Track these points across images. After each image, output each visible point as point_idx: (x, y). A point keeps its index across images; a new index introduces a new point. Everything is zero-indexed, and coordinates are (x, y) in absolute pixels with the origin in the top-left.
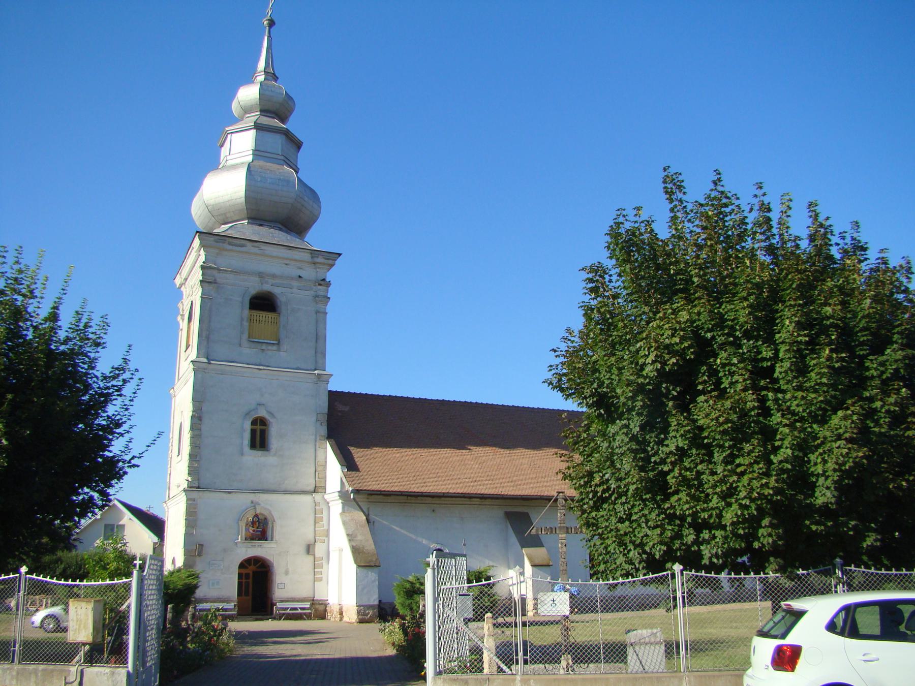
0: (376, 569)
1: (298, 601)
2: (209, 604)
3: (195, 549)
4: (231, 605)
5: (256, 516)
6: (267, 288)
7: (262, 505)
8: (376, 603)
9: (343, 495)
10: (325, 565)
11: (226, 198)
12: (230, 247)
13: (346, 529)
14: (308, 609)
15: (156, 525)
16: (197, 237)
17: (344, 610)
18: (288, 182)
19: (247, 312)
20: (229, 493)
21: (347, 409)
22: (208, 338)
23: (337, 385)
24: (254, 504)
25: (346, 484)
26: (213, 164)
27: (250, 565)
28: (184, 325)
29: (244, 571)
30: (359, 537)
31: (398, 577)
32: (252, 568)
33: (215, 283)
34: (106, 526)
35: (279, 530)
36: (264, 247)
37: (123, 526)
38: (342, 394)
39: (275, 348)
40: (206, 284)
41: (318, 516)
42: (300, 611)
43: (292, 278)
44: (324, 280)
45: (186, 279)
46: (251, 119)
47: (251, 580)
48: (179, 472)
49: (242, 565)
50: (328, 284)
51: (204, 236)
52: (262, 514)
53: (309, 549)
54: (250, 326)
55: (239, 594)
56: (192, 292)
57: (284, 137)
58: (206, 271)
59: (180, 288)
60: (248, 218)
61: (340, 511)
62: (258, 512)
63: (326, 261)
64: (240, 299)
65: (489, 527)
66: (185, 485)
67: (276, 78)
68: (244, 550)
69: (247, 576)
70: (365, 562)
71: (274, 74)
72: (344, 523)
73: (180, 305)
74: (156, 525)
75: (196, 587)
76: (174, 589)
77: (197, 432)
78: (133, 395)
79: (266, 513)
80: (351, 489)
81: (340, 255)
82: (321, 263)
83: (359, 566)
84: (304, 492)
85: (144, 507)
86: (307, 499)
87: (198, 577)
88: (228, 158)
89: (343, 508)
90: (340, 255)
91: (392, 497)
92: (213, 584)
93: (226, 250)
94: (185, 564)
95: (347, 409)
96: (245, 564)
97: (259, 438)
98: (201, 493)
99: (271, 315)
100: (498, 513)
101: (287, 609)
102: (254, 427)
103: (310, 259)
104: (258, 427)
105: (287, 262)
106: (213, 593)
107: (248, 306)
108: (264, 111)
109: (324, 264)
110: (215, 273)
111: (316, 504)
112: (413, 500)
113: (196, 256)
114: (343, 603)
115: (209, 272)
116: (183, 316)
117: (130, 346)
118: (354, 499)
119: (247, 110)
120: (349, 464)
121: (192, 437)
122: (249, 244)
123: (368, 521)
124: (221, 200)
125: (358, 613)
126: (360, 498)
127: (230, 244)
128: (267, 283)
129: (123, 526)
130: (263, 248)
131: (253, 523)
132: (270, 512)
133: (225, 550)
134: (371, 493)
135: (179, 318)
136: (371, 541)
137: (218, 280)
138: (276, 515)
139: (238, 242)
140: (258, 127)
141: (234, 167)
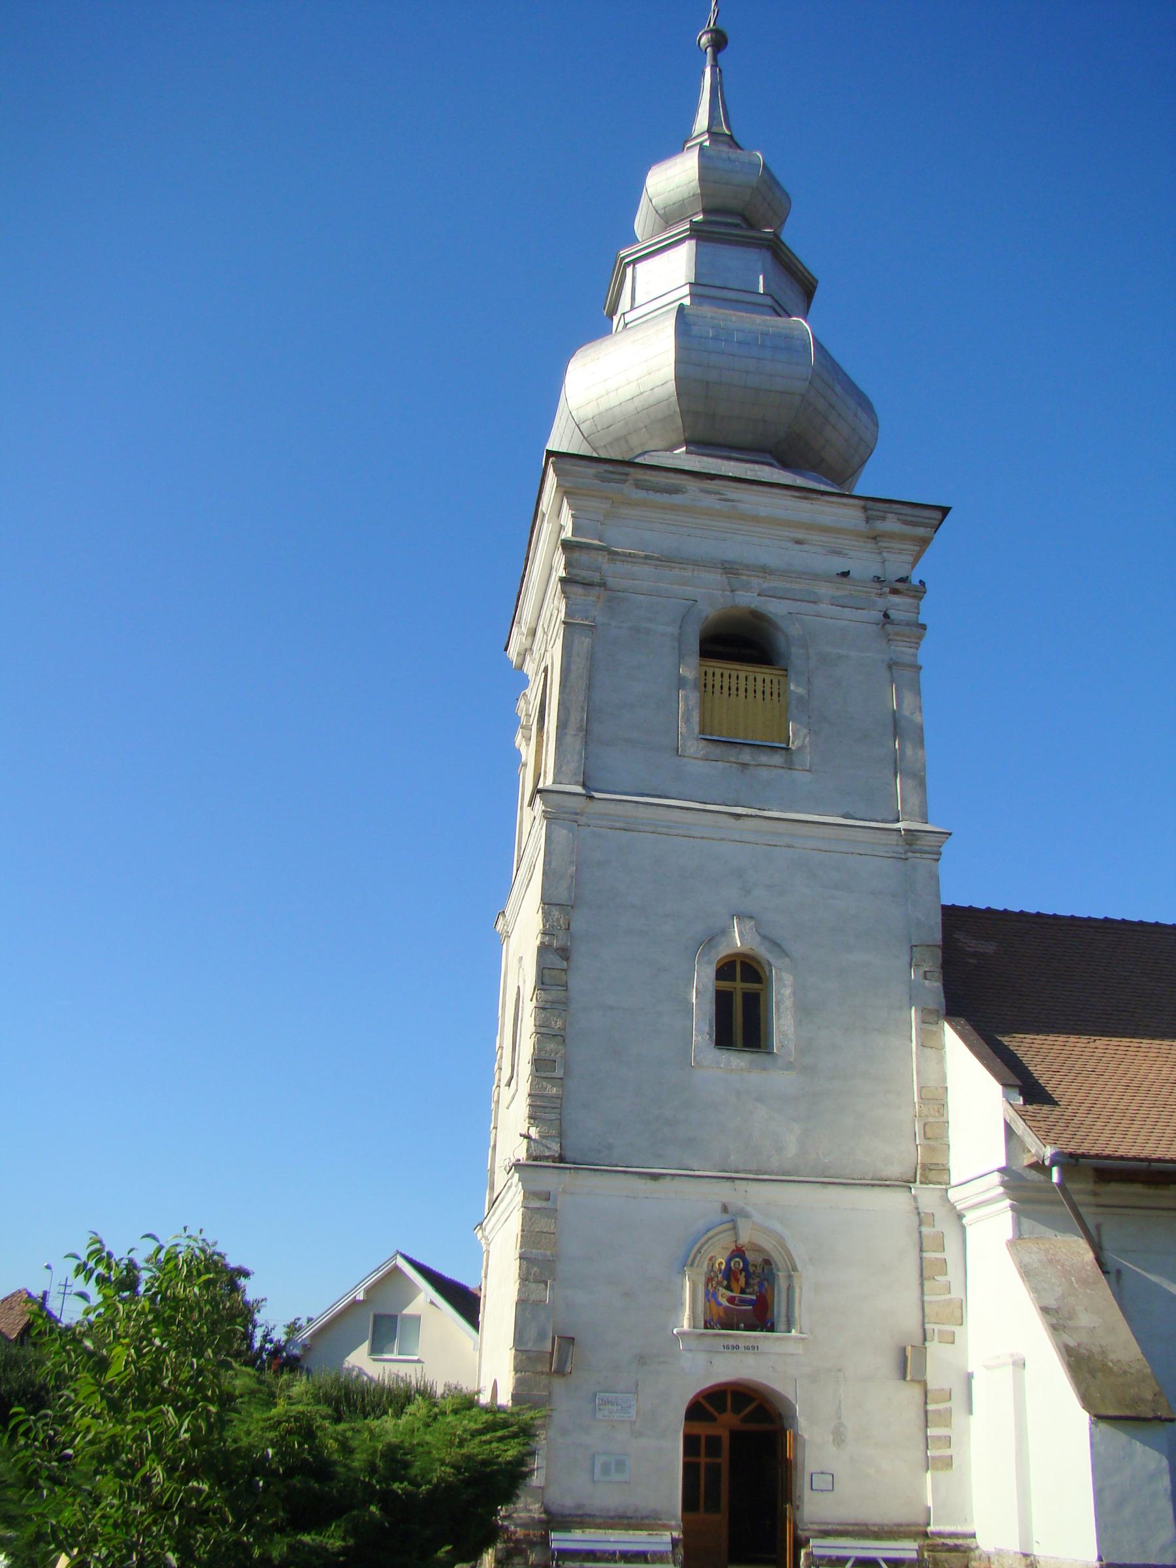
3: (548, 1353)
4: (663, 1540)
5: (739, 1252)
6: (747, 599)
7: (757, 1217)
9: (1022, 1187)
10: (957, 1417)
11: (627, 392)
12: (641, 494)
15: (466, 1302)
19: (690, 670)
20: (655, 1177)
21: (989, 948)
22: (587, 732)
23: (948, 902)
24: (731, 1216)
26: (595, 318)
27: (722, 1409)
28: (528, 753)
29: (703, 1429)
30: (1085, 1319)
32: (727, 1422)
33: (603, 585)
34: (377, 1318)
35: (810, 1295)
37: (417, 1319)
38: (970, 913)
39: (777, 759)
40: (579, 590)
41: (931, 1254)
43: (816, 577)
44: (903, 580)
45: (533, 633)
47: (724, 1460)
48: (512, 1128)
49: (697, 1411)
50: (919, 591)
51: (567, 465)
52: (759, 1249)
53: (908, 1363)
54: (702, 702)
55: (690, 1503)
57: (768, 255)
58: (576, 555)
59: (520, 667)
60: (688, 442)
61: (1008, 1232)
62: (744, 1239)
63: (908, 530)
64: (673, 630)
68: (701, 1358)
69: (713, 1444)
71: (731, 137)
72: (1027, 1273)
73: (522, 704)
74: (466, 1302)
77: (555, 994)
79: (768, 1244)
80: (1048, 1151)
81: (945, 511)
82: (891, 536)
83: (1099, 1418)
84: (882, 1183)
86: (896, 1200)
89: (1017, 1225)
90: (945, 511)
92: (606, 1469)
94: (515, 1397)
95: (989, 948)
96: (707, 1406)
97: (741, 1019)
98: (567, 1177)
99: (762, 674)
102: (726, 985)
103: (862, 525)
104: (739, 986)
106: (606, 1498)
107: (696, 647)
109: (902, 537)
110: (602, 559)
111: (921, 1218)
113: (557, 519)
114: (1037, 1551)
115: (583, 557)
118: (1061, 1185)
119: (668, 217)
120: (1027, 1088)
121: (540, 1009)
122: (692, 485)
124: (613, 400)
126: (1081, 1188)
127: (638, 485)
128: (747, 587)
129: (417, 1319)
131: (729, 1275)
133: (642, 1360)
135: (519, 740)
137: (611, 581)
138: (799, 1252)
141: (648, 319)
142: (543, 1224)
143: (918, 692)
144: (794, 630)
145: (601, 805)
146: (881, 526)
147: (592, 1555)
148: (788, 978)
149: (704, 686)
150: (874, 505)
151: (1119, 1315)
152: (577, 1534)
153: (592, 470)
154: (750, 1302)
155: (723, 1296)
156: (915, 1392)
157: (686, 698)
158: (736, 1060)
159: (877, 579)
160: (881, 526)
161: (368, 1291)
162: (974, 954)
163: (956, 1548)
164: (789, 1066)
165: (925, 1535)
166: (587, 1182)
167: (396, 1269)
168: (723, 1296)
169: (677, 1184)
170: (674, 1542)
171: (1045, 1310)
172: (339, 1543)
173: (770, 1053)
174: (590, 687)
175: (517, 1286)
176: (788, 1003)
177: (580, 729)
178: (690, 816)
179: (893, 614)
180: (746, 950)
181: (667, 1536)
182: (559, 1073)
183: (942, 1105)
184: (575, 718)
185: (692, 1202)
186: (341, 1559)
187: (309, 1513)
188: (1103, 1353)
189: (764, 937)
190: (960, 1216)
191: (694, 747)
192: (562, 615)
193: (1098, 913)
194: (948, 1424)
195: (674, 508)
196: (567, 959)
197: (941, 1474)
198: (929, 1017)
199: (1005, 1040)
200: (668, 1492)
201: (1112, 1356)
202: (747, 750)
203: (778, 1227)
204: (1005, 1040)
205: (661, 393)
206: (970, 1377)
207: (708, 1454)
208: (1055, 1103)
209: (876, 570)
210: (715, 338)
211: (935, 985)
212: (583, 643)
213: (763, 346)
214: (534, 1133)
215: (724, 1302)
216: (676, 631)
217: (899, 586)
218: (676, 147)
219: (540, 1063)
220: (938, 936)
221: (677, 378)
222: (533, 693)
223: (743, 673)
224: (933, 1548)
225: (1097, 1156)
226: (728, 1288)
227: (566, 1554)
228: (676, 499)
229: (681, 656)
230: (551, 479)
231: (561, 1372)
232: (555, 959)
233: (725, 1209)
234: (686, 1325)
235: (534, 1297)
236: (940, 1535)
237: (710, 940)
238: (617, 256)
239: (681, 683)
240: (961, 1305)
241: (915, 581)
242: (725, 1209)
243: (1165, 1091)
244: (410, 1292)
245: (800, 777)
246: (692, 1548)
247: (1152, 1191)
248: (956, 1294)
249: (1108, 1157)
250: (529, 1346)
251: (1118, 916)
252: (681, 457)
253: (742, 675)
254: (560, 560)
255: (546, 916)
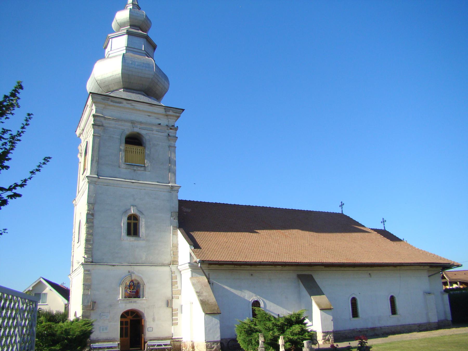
0: (218, 315)
1: (162, 340)
2: (100, 344)
3: (90, 305)
4: (116, 344)
5: (132, 281)
6: (136, 130)
7: (136, 274)
8: (219, 339)
9: (193, 266)
12: (112, 103)
13: (195, 288)
14: (169, 345)
15: (65, 292)
16: (90, 97)
17: (195, 345)
18: (149, 64)
19: (123, 147)
21: (189, 210)
22: (98, 162)
24: (131, 274)
25: (195, 257)
26: (100, 54)
27: (128, 315)
28: (82, 159)
29: (124, 320)
30: (205, 294)
31: (238, 320)
32: (129, 318)
33: (102, 126)
35: (148, 290)
36: (134, 104)
37: (46, 294)
39: (142, 169)
40: (97, 127)
42: (163, 347)
43: (153, 125)
45: (83, 130)
46: (124, 30)
47: (129, 326)
48: (79, 253)
49: (123, 316)
50: (176, 129)
51: (95, 96)
52: (137, 280)
53: (169, 303)
54: (125, 155)
55: (121, 336)
56: (86, 133)
57: (145, 40)
58: (96, 118)
59: (79, 137)
60: (124, 88)
61: (190, 276)
62: (133, 278)
63: (175, 114)
65: (287, 285)
66: (83, 261)
67: (139, 9)
68: (124, 305)
69: (126, 323)
70: (210, 311)
71: (138, 5)
72: (194, 284)
73: (80, 147)
74: (65, 292)
75: (90, 332)
76: (73, 335)
77: (91, 224)
78: (20, 130)
79: (139, 279)
80: (198, 260)
81: (183, 110)
84: (163, 265)
85: (59, 283)
86: (167, 269)
87: (92, 325)
88: (110, 53)
90: (183, 110)
91: (225, 266)
93: (110, 105)
94: (83, 316)
95: (189, 210)
97: (133, 229)
98: (93, 266)
99: (139, 148)
100: (292, 275)
101: (154, 345)
102: (129, 221)
104: (132, 221)
105: (149, 114)
106: (103, 336)
108: (132, 26)
110: (102, 120)
112: (238, 268)
113: (91, 109)
115: (98, 119)
116: (81, 153)
117: (29, 115)
118: (200, 267)
119: (121, 25)
120: (195, 245)
122: (125, 102)
123: (209, 282)
125: (207, 347)
126: (205, 267)
127: (112, 101)
128: (137, 127)
129: (46, 294)
130: (134, 104)
131: (130, 286)
132: (142, 279)
133: (111, 306)
134: (211, 263)
135: (79, 156)
136: (213, 296)
137: (105, 125)
138: (145, 281)
139: (117, 100)
140: (129, 33)
142: (88, 277)
143: (175, 153)
144: (147, 137)
145: (102, 180)
146: (168, 113)
147: (100, 348)
148: (144, 220)
149: (126, 151)
150: (167, 108)
151: (212, 292)
152: (97, 344)
153: (100, 97)
154: (134, 292)
155: (129, 291)
156: (170, 309)
157: (122, 154)
158: (132, 239)
159: (167, 125)
160: (168, 113)
161: (33, 287)
162: (186, 212)
163: (178, 341)
164: (144, 240)
165: (172, 339)
166: (98, 267)
167: (40, 282)
168: (129, 291)
169: (118, 267)
170: (118, 344)
171: (197, 292)
172: (59, 348)
173: (139, 237)
174: (99, 151)
175: (82, 291)
176: (144, 225)
177: (96, 161)
178: (121, 182)
179: (170, 134)
180: (134, 213)
181: (117, 343)
182: (91, 243)
183: (177, 248)
184: (95, 159)
185: (122, 271)
186: (464, 291)
187: (55, 343)
188: (208, 301)
189: (138, 211)
190: (180, 272)
191: (123, 166)
192: (92, 133)
193: (214, 202)
194: (177, 316)
195: (120, 107)
196: (93, 216)
197: (175, 326)
198: (175, 228)
199: (191, 233)
200: (116, 333)
201: (210, 301)
202: (135, 167)
203: (141, 275)
204: (191, 233)
205: (118, 76)
206: (182, 306)
207: (125, 325)
208: (201, 248)
209: (166, 123)
210: (131, 64)
211: (176, 221)
212: (97, 140)
213: (143, 66)
214: (86, 256)
215: (129, 292)
216: (119, 137)
217: (172, 127)
218: (123, 7)
219: (87, 241)
220: (177, 210)
221: (122, 73)
222: (83, 145)
223: (135, 147)
224: (173, 341)
225: (208, 261)
226: (130, 289)
227: (95, 348)
228: (120, 105)
229: (121, 143)
230: (90, 98)
231: (93, 309)
232: (91, 217)
233: (129, 272)
234: (120, 298)
235: (86, 293)
236: (175, 339)
237: (126, 212)
238: (107, 35)
239: (120, 150)
240: (180, 291)
241: (176, 126)
242: (129, 272)
243: (224, 245)
244: (45, 287)
245: (147, 173)
246: (122, 344)
247: (220, 266)
248: (179, 288)
249: (210, 261)
250: (86, 304)
251: (218, 202)
252: (121, 93)
253: (135, 148)
254: (92, 119)
255: (88, 206)
